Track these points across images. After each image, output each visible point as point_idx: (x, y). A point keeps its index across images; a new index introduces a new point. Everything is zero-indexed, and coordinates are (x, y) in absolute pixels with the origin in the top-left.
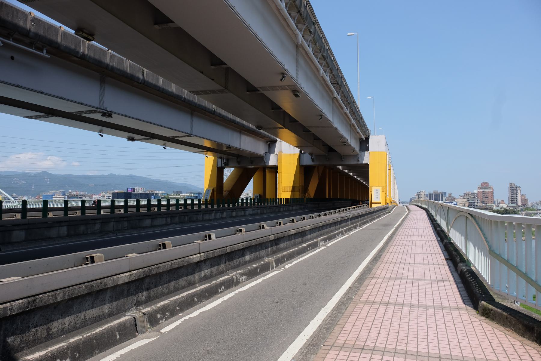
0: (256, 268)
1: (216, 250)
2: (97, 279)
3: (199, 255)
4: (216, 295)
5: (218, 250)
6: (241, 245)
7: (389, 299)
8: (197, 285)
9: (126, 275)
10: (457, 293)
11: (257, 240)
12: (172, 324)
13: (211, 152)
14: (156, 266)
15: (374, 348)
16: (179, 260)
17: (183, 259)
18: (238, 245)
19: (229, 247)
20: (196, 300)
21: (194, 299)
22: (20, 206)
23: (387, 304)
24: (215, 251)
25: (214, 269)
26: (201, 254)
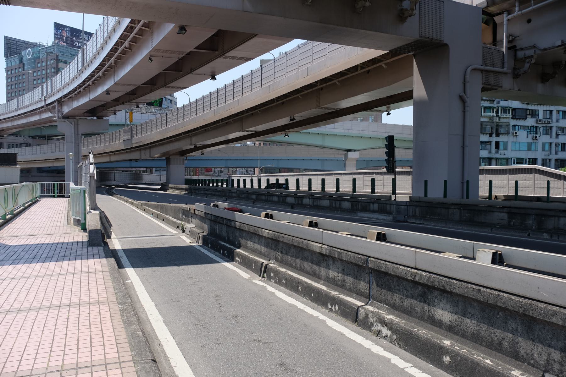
0: (442, 350)
1: (346, 252)
2: (476, 283)
3: (320, 245)
4: (323, 306)
5: (350, 253)
6: (403, 269)
7: (71, 300)
8: (322, 282)
9: (410, 270)
10: (26, 212)
11: (502, 294)
12: (351, 331)
13: (518, 102)
14: (283, 235)
15: (77, 366)
16: (299, 239)
17: (304, 240)
18: (387, 265)
19: (373, 259)
20: (300, 290)
21: (298, 286)
22: (275, 182)
23: (71, 304)
24: (343, 251)
25: (350, 280)
26: (324, 246)
